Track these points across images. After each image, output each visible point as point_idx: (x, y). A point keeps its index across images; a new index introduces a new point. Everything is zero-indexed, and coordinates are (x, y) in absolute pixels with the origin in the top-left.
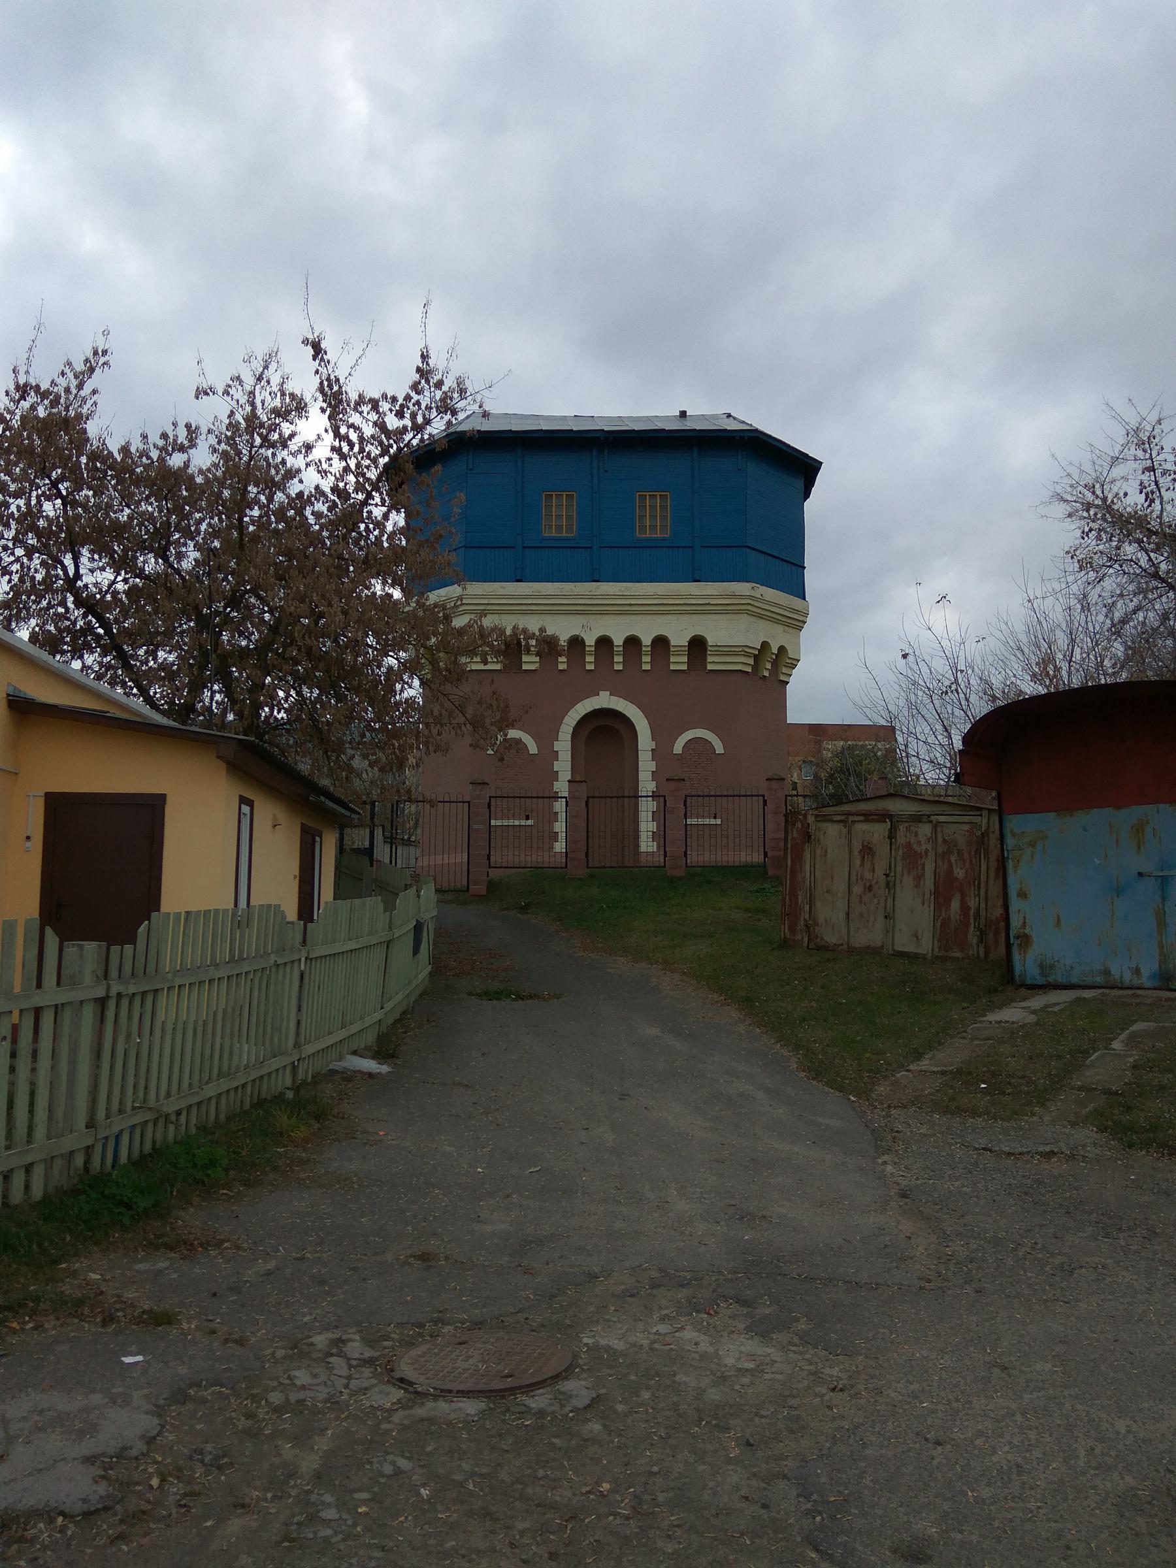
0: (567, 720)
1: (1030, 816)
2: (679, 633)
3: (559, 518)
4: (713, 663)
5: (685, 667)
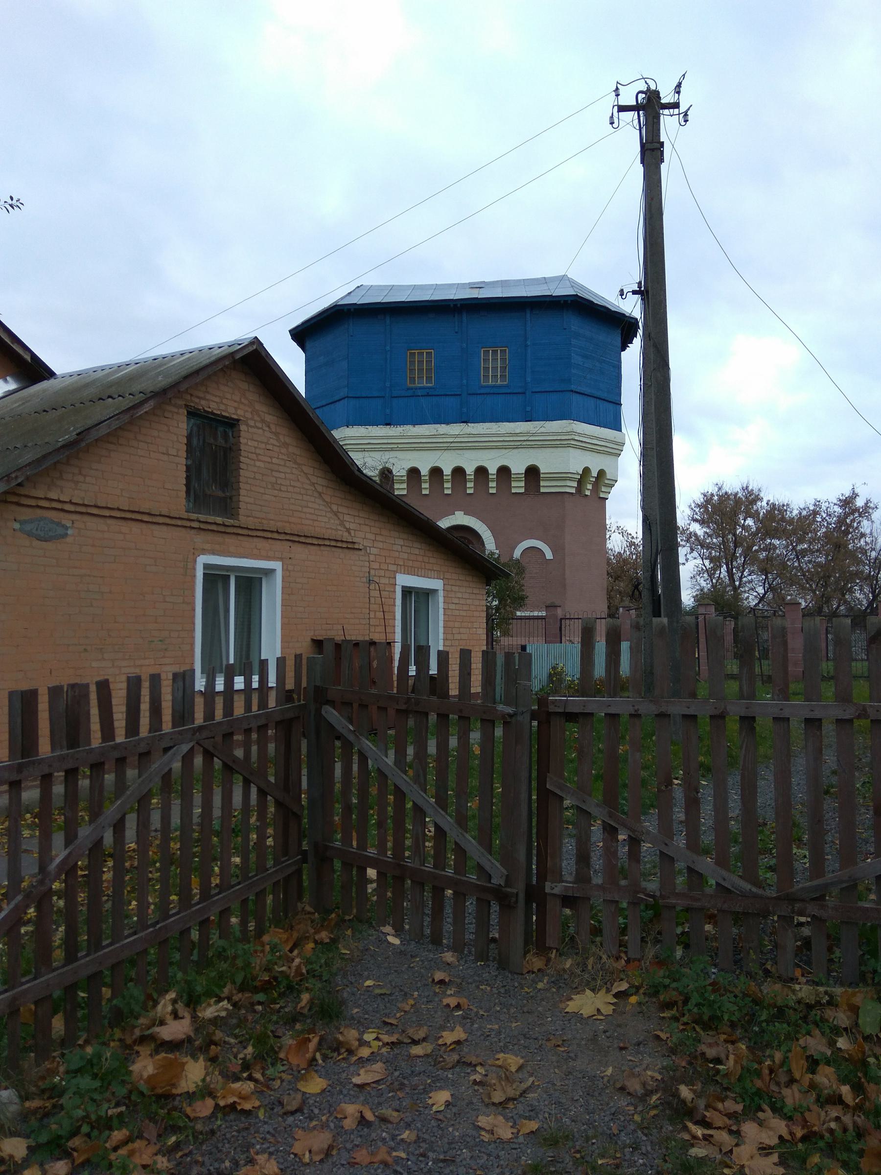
0: (485, 527)
1: (39, 717)
2: (518, 466)
3: (492, 368)
4: (545, 487)
5: (522, 490)
